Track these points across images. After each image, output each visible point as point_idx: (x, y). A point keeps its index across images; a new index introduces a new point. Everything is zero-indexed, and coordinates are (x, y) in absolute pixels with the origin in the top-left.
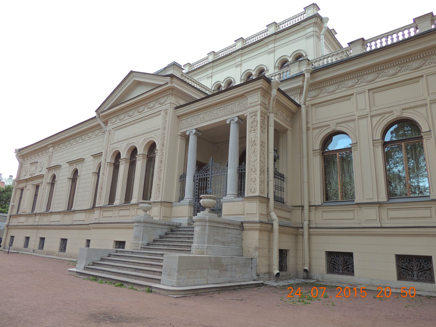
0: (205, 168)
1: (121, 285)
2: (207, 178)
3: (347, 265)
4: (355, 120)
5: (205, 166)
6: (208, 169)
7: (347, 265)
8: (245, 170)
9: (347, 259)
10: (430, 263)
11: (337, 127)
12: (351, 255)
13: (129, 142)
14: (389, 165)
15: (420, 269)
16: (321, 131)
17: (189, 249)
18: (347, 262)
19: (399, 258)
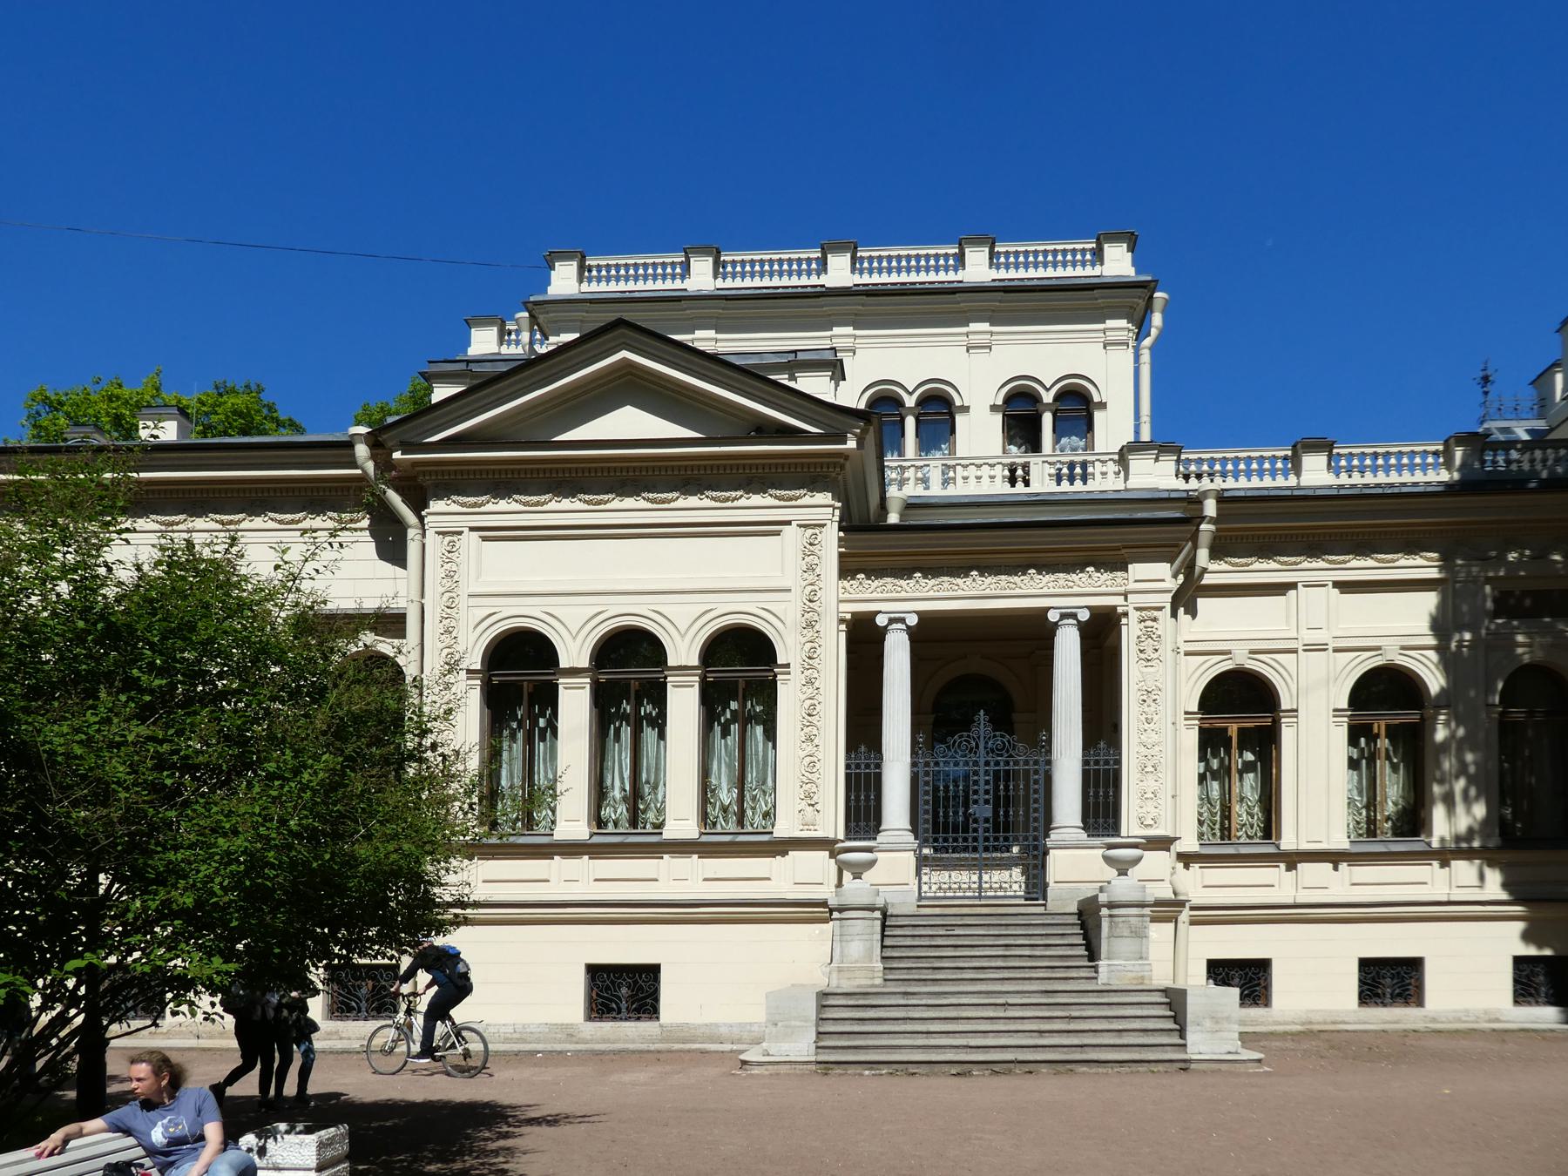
0: (955, 742)
1: (967, 1074)
3: (1251, 987)
4: (1295, 651)
6: (972, 748)
7: (1251, 987)
8: (848, 766)
9: (1253, 973)
10: (1265, 972)
12: (653, 971)
13: (713, 606)
14: (180, 815)
17: (1094, 975)
19: (594, 971)
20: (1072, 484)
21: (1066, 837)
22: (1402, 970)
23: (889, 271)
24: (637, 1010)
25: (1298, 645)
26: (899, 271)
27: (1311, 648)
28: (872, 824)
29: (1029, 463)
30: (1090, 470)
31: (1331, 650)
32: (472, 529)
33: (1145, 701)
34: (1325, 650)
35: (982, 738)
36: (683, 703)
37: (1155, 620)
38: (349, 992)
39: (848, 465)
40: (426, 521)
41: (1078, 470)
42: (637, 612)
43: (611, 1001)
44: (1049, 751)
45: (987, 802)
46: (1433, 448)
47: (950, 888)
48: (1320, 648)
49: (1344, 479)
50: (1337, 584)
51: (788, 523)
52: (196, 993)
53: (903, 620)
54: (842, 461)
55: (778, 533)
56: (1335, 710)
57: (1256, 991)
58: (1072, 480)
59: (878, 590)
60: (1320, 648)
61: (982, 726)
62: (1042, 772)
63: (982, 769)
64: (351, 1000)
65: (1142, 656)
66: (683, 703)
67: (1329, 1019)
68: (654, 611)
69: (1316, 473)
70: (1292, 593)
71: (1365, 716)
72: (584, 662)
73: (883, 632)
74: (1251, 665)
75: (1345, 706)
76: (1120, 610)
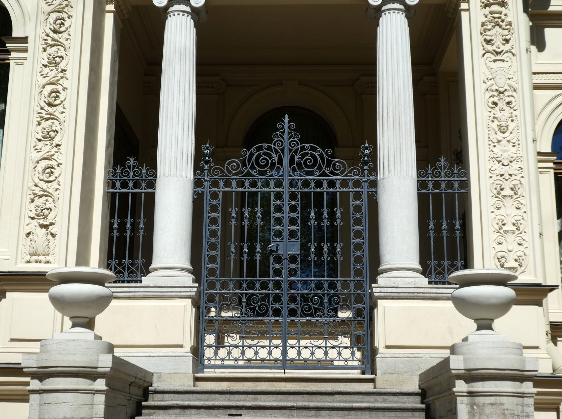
0: (251, 155)
2: (266, 197)
6: (273, 164)
21: (401, 282)
28: (140, 262)
33: (495, 104)
44: (374, 169)
45: (292, 234)
61: (286, 136)
62: (365, 196)
63: (286, 191)
65: (489, 48)
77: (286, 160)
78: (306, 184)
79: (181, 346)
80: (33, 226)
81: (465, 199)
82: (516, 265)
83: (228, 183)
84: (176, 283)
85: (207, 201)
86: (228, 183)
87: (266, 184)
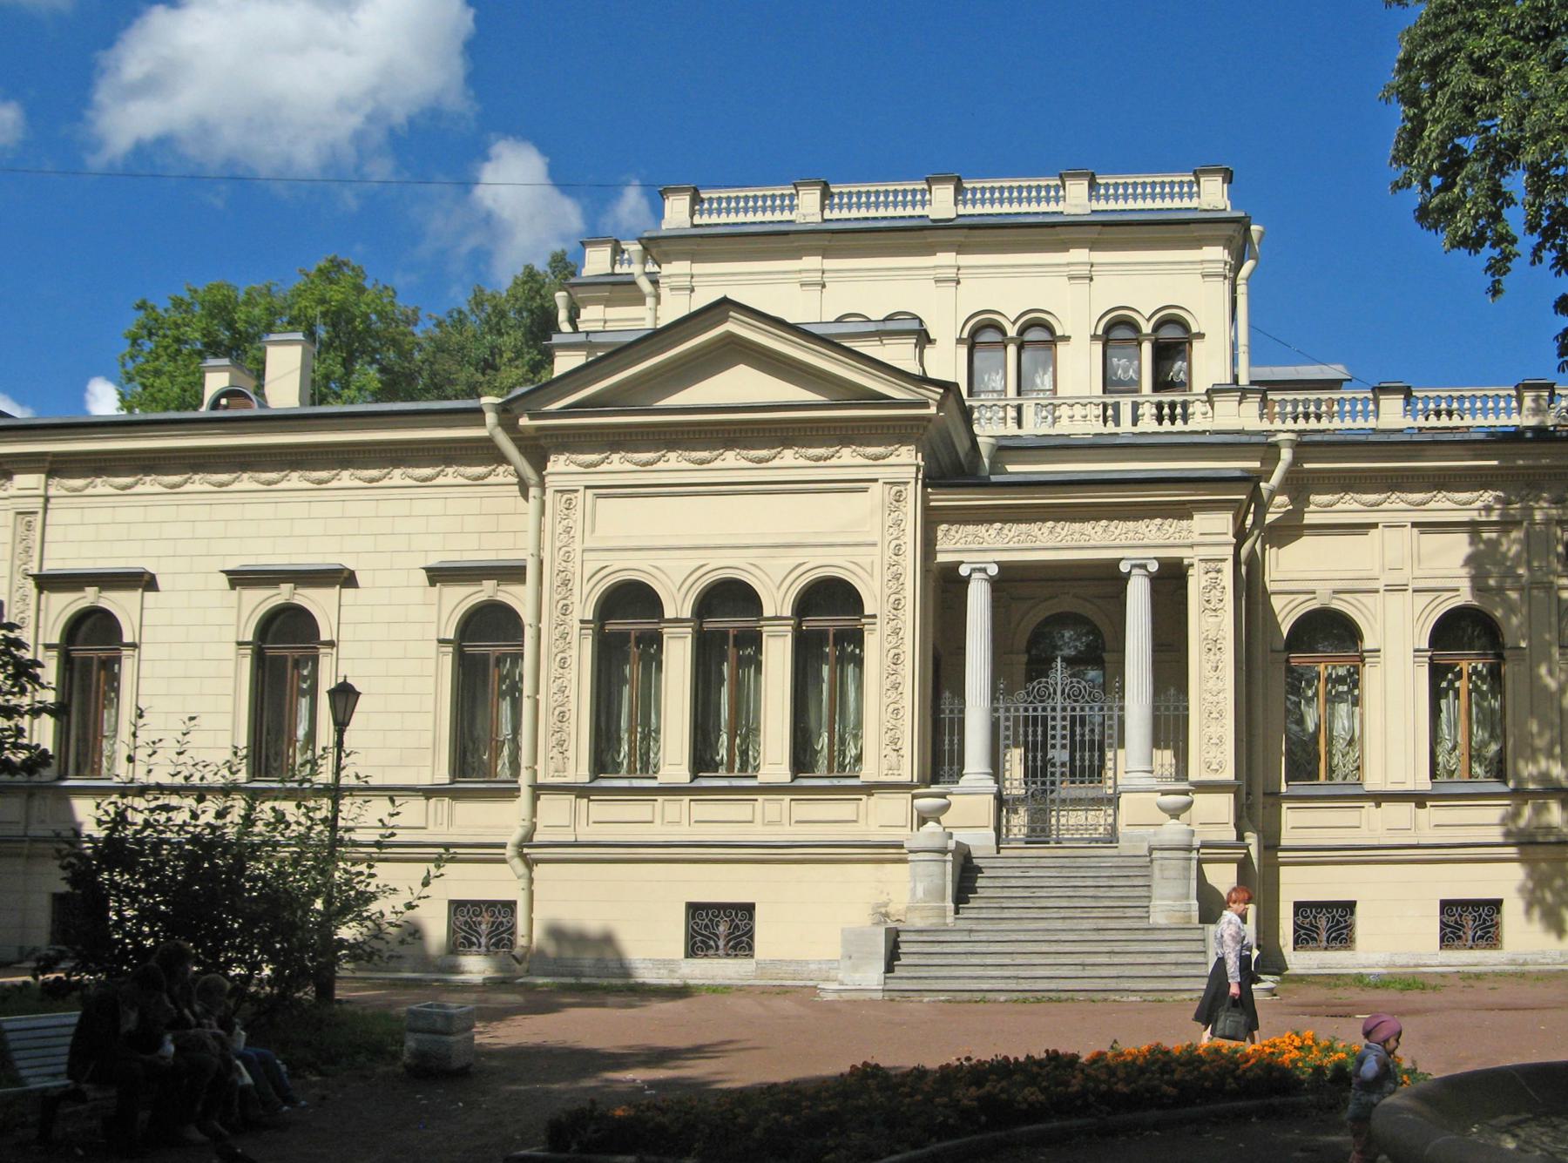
0: (1034, 688)
2: (1045, 718)
3: (1338, 930)
4: (1377, 591)
5: (1035, 683)
6: (1050, 694)
7: (1338, 930)
10: (512, 916)
11: (1334, 601)
15: (1332, 927)
16: (1290, 602)
18: (1338, 922)
19: (694, 909)
20: (1173, 423)
21: (1136, 782)
22: (1484, 911)
23: (1001, 202)
24: (734, 948)
25: (1380, 585)
26: (1011, 202)
27: (1392, 589)
28: (956, 767)
29: (1119, 403)
30: (1190, 410)
31: (1411, 590)
32: (587, 487)
33: (1210, 650)
34: (1406, 590)
35: (1059, 684)
36: (778, 654)
37: (1219, 571)
38: (470, 928)
39: (931, 426)
40: (547, 479)
41: (1179, 410)
42: (738, 566)
43: (710, 938)
44: (1123, 698)
45: (1064, 747)
46: (1505, 393)
47: (1086, 830)
48: (1401, 589)
49: (1421, 422)
50: (1414, 525)
51: (876, 480)
52: (366, 911)
53: (984, 570)
54: (925, 423)
55: (865, 490)
56: (1416, 651)
57: (1343, 934)
58: (1173, 419)
59: (961, 541)
60: (1401, 589)
61: (1059, 672)
62: (1116, 718)
63: (1059, 714)
64: (472, 935)
65: (1208, 606)
66: (778, 654)
67: (1412, 962)
68: (752, 564)
69: (1392, 415)
70: (1373, 531)
71: (1446, 657)
72: (687, 613)
73: (965, 581)
74: (1337, 605)
75: (1426, 646)
76: (1186, 562)
77: (1059, 692)
78: (1073, 709)
79: (1288, 808)
80: (888, 750)
81: (1187, 717)
82: (1218, 767)
83: (1017, 710)
84: (664, 972)
85: (1002, 724)
86: (1017, 710)
87: (1044, 709)
